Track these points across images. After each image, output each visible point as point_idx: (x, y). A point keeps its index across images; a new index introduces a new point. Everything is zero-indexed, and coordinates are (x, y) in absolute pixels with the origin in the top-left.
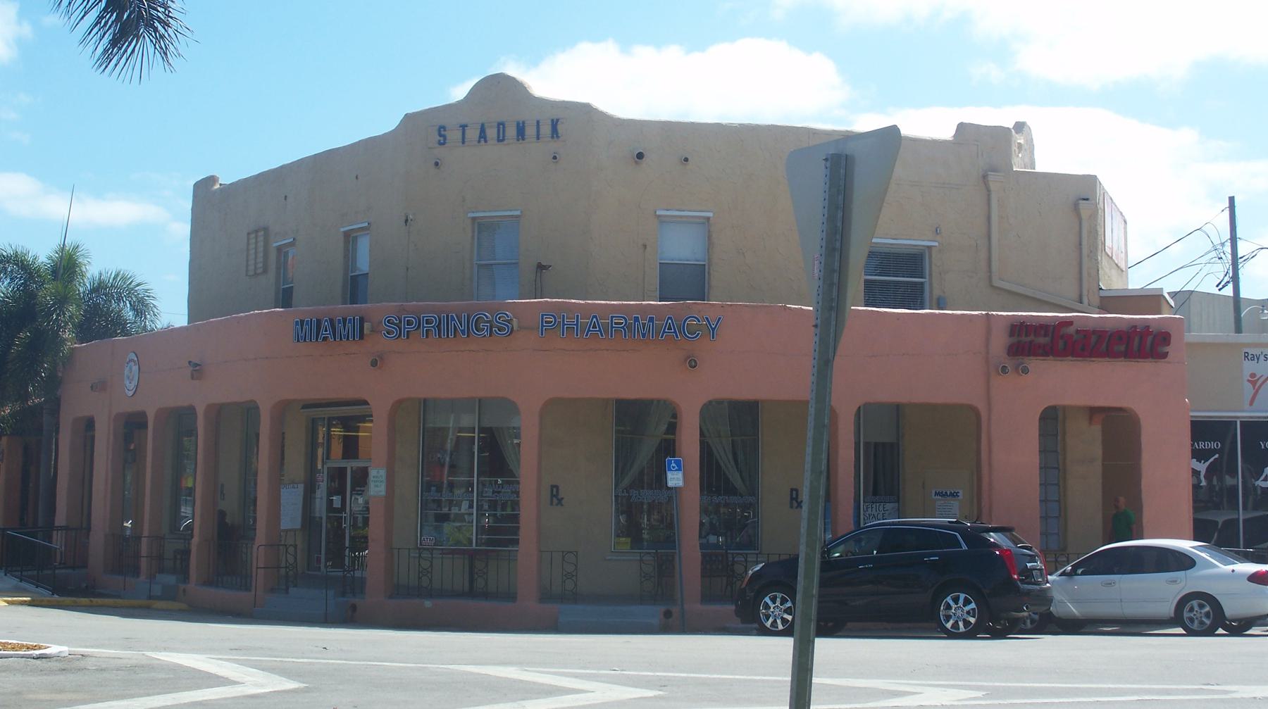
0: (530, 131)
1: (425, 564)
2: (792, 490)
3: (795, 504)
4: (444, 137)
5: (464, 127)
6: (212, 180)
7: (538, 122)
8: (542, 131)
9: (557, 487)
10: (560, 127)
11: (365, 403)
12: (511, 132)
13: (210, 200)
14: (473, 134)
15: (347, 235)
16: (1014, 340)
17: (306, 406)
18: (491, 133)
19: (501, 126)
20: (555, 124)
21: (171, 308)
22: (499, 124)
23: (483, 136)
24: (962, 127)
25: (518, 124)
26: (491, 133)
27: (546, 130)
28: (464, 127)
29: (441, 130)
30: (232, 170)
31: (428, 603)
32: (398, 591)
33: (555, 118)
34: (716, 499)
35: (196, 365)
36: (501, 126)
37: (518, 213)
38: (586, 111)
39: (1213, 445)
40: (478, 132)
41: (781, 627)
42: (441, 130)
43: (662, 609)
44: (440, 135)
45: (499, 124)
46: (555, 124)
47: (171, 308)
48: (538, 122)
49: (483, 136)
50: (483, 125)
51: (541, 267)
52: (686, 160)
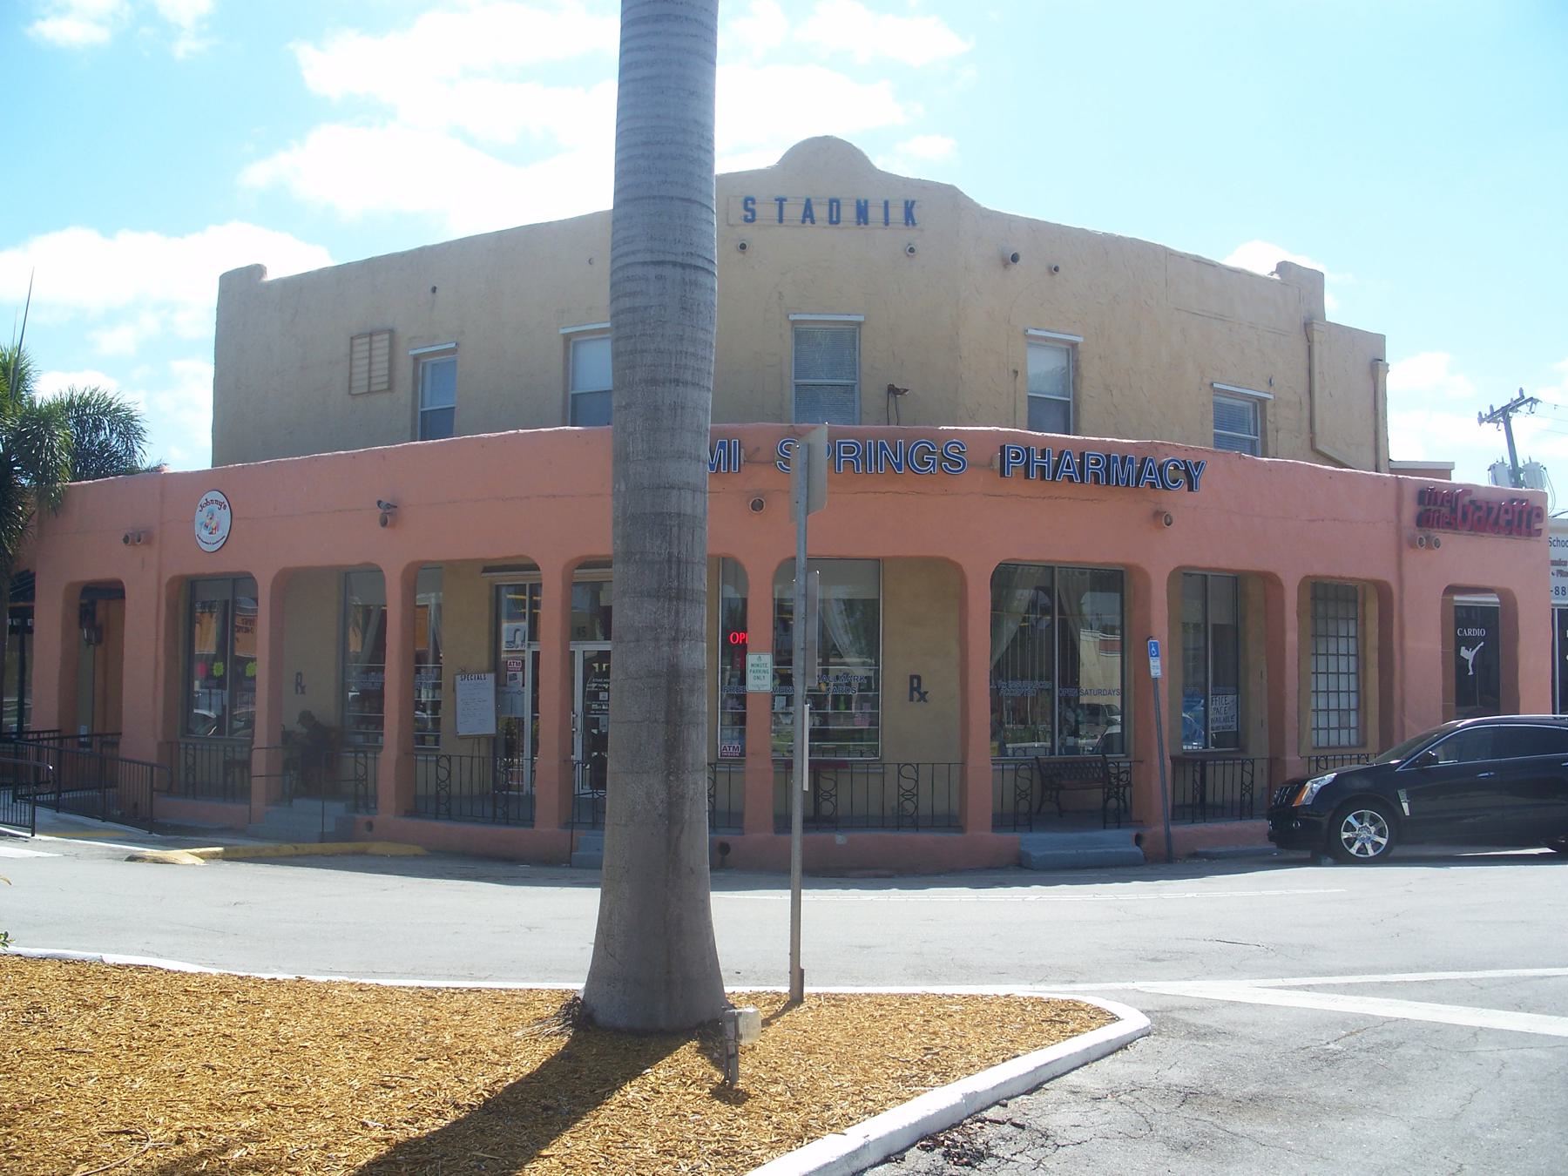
0: (875, 213)
1: (908, 785)
2: (912, 678)
3: (916, 695)
4: (753, 212)
5: (781, 201)
6: (257, 270)
7: (886, 203)
8: (892, 217)
9: (919, 678)
10: (915, 212)
11: (535, 568)
12: (848, 213)
13: (242, 294)
14: (794, 211)
15: (567, 338)
16: (1422, 508)
17: (486, 570)
18: (821, 212)
19: (834, 204)
20: (909, 208)
21: (178, 433)
22: (831, 201)
23: (808, 214)
24: (1283, 267)
25: (858, 202)
26: (821, 212)
27: (897, 214)
28: (781, 201)
29: (748, 202)
30: (288, 258)
31: (840, 839)
32: (430, 804)
33: (910, 199)
34: (855, 684)
35: (389, 506)
36: (834, 204)
37: (862, 319)
38: (950, 197)
39: (1479, 632)
40: (802, 209)
41: (1371, 853)
42: (748, 202)
43: (1132, 833)
44: (747, 209)
45: (831, 201)
46: (909, 208)
47: (178, 433)
48: (886, 203)
49: (808, 214)
50: (808, 201)
51: (893, 391)
52: (1056, 269)
